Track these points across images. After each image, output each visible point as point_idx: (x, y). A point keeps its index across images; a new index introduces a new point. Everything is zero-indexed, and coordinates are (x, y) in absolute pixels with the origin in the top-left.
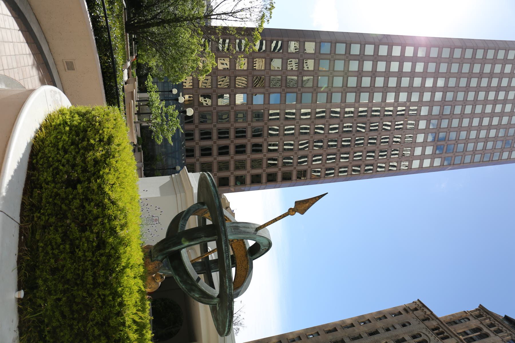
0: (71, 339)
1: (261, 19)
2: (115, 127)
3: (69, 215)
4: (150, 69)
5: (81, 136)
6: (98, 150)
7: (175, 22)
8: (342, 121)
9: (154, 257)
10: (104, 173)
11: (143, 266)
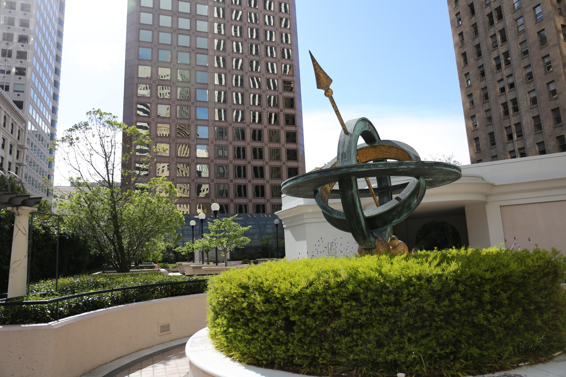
0: (450, 328)
1: (112, 125)
2: (229, 281)
3: (322, 329)
4: (169, 249)
5: (239, 316)
6: (254, 299)
7: (116, 220)
8: (229, 38)
9: (371, 246)
10: (278, 293)
11: (380, 255)
